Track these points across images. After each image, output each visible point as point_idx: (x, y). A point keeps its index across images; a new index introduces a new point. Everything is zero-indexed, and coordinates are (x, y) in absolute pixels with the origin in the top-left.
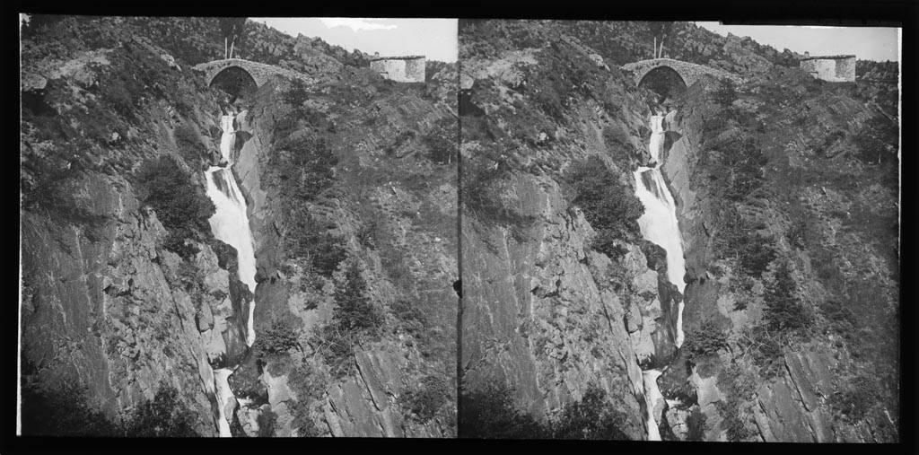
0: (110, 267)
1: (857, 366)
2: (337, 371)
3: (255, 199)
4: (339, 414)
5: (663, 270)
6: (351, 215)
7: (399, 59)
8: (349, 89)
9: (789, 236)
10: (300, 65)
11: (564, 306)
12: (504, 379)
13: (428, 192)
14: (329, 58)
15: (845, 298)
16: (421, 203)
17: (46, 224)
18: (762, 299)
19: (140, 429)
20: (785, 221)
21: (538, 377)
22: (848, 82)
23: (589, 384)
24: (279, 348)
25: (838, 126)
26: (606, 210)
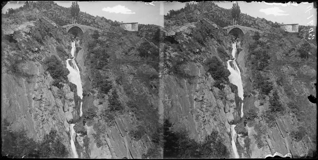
0: (196, 92)
1: (139, 122)
2: (109, 124)
3: (243, 70)
4: (110, 138)
5: (76, 92)
6: (274, 75)
7: (290, 25)
8: (274, 35)
9: (116, 81)
10: (258, 27)
11: (43, 103)
12: (24, 127)
13: (300, 68)
14: (107, 23)
15: (135, 100)
16: (297, 71)
17: (14, 77)
18: (108, 101)
19: (206, 144)
20: (115, 76)
21: (35, 126)
22: (135, 31)
23: (52, 128)
24: (251, 118)
25: (132, 45)
26: (57, 73)
